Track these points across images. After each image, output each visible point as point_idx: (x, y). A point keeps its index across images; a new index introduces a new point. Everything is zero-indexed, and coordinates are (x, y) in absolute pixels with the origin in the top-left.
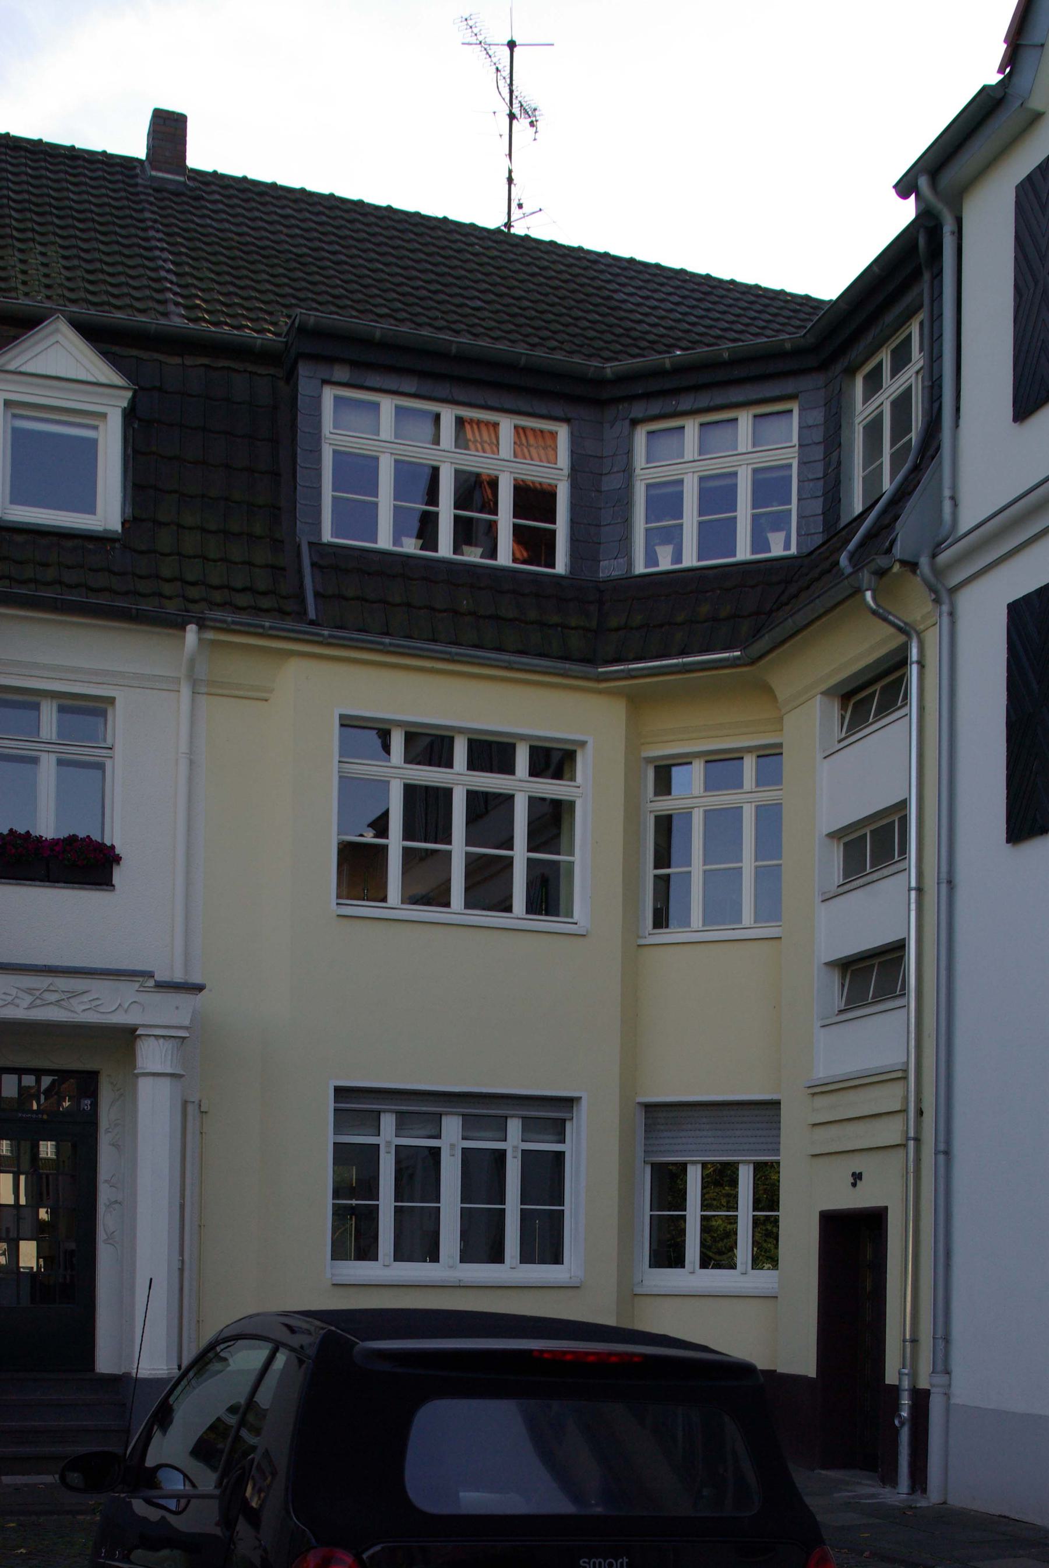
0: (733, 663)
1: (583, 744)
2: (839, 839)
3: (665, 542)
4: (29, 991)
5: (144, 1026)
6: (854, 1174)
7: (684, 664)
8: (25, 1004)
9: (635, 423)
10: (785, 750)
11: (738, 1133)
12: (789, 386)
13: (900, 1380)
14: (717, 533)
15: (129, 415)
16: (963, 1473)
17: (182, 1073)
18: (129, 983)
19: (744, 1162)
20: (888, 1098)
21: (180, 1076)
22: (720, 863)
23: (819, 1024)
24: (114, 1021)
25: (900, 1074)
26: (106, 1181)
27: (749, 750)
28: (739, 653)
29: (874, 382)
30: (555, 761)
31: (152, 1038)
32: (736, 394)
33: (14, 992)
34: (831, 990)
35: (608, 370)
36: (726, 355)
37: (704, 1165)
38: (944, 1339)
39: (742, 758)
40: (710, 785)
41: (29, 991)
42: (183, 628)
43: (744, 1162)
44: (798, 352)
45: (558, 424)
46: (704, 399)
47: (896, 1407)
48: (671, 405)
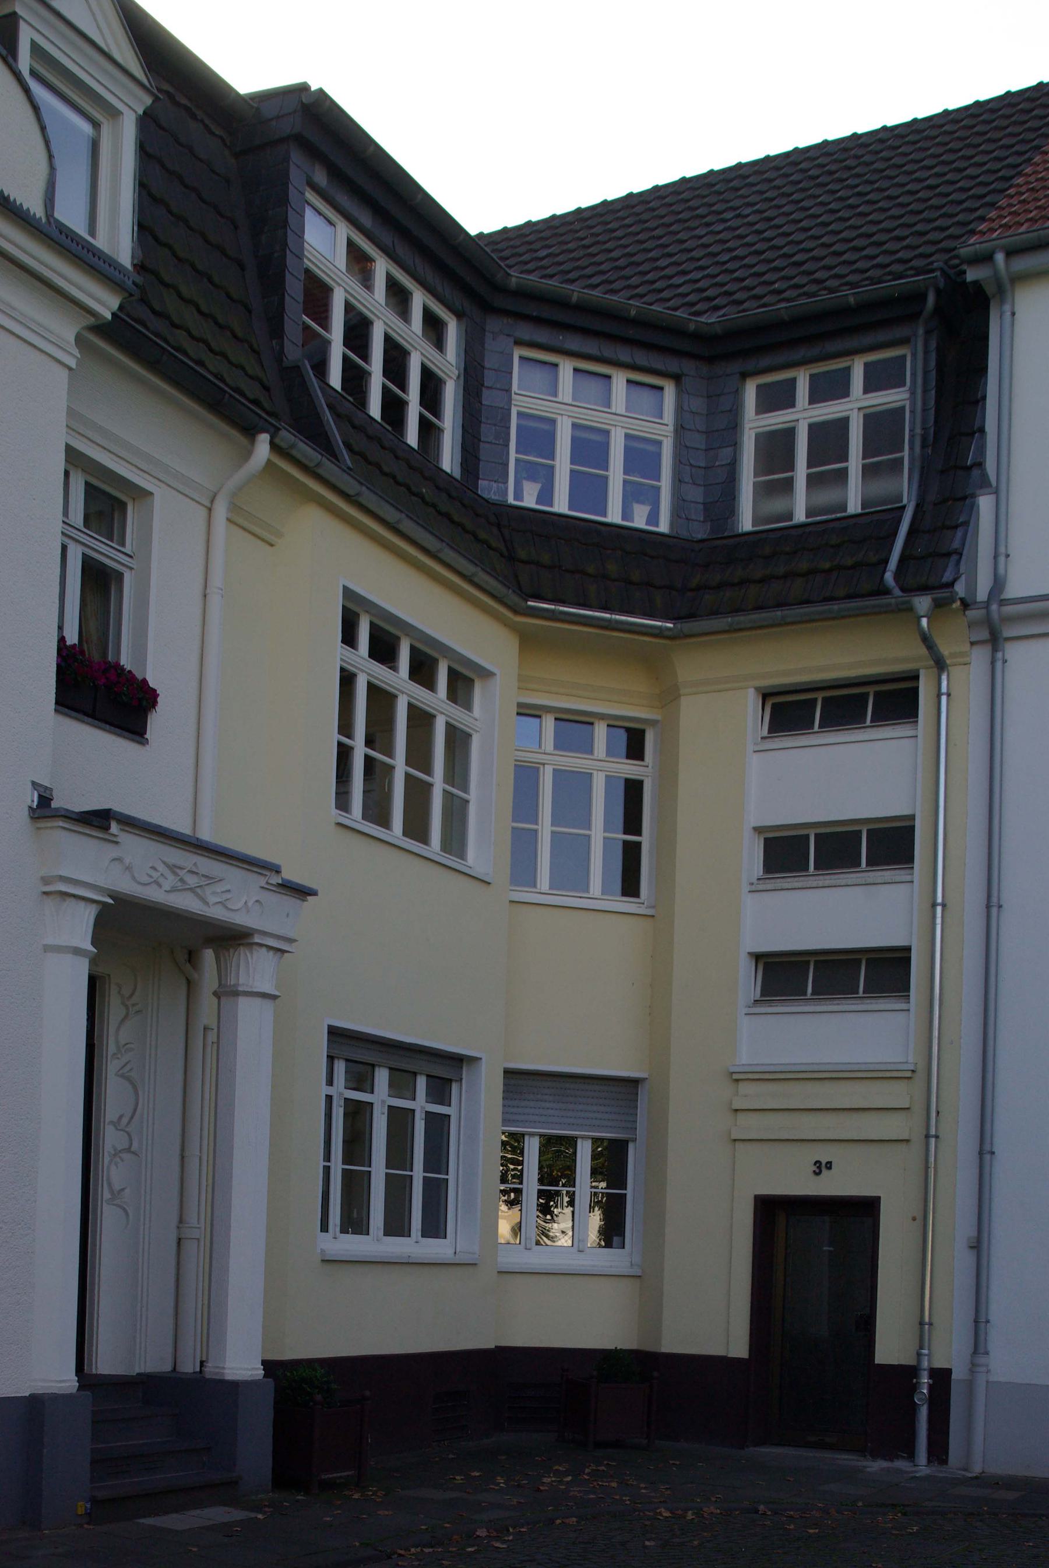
0: (659, 633)
1: (486, 674)
2: (760, 833)
3: (532, 478)
4: (173, 868)
5: (265, 934)
6: (818, 1163)
7: (610, 621)
8: (167, 886)
9: (744, 376)
10: (515, 710)
11: (581, 1107)
12: (673, 365)
13: (919, 1361)
14: (589, 487)
15: (147, 121)
16: (989, 1444)
17: (277, 993)
18: (255, 876)
19: (583, 1137)
20: (895, 1094)
21: (274, 997)
22: (573, 828)
23: (746, 1011)
24: (238, 922)
25: (909, 1074)
26: (111, 1122)
27: (602, 717)
28: (671, 625)
29: (777, 398)
30: (461, 685)
31: (264, 949)
32: (624, 354)
33: (161, 868)
34: (747, 981)
35: (514, 280)
36: (633, 313)
37: (596, 1141)
38: (979, 1323)
39: (592, 724)
40: (560, 744)
41: (173, 868)
42: (250, 432)
43: (583, 1137)
44: (697, 336)
45: (450, 315)
46: (591, 347)
47: (914, 1388)
48: (608, 350)
